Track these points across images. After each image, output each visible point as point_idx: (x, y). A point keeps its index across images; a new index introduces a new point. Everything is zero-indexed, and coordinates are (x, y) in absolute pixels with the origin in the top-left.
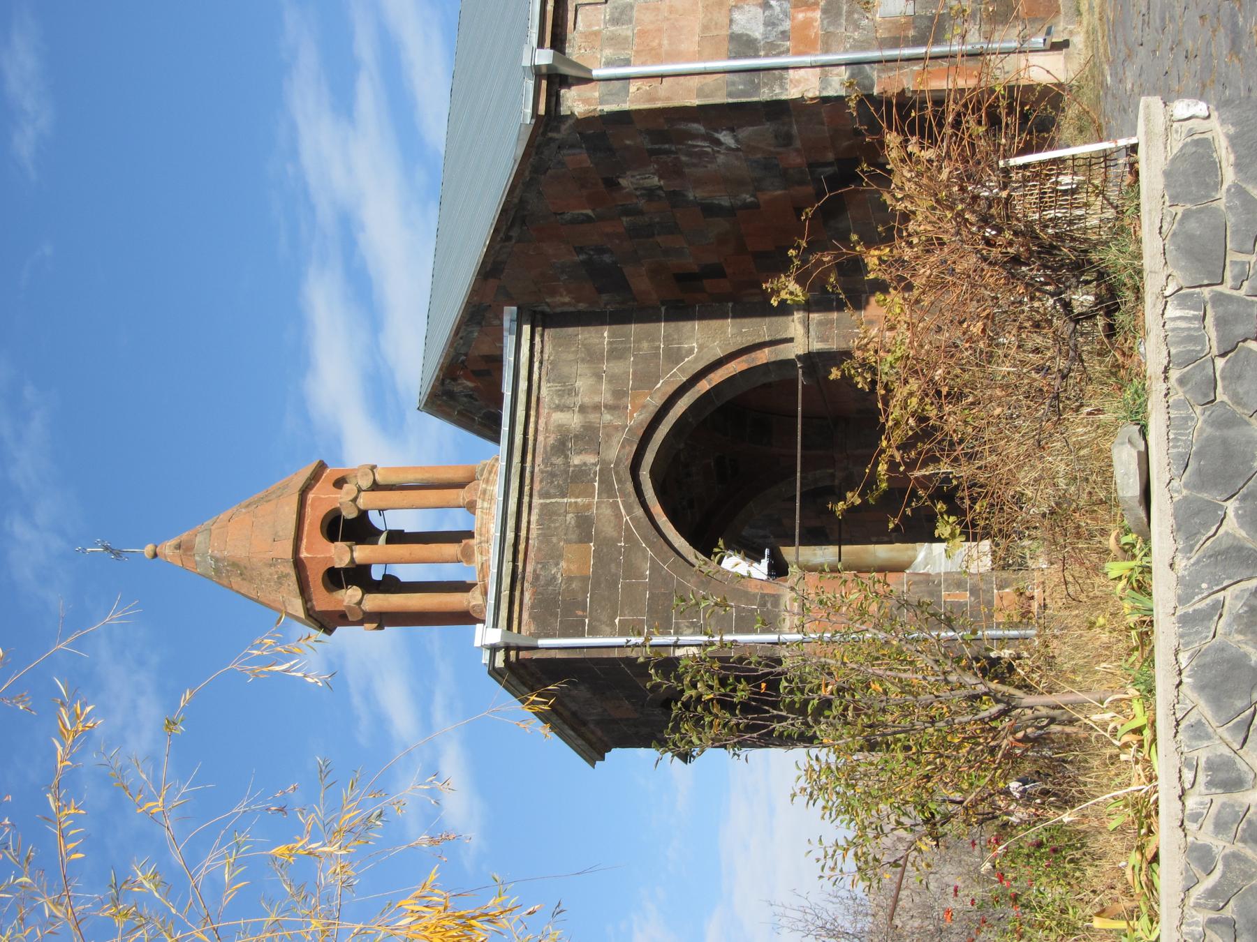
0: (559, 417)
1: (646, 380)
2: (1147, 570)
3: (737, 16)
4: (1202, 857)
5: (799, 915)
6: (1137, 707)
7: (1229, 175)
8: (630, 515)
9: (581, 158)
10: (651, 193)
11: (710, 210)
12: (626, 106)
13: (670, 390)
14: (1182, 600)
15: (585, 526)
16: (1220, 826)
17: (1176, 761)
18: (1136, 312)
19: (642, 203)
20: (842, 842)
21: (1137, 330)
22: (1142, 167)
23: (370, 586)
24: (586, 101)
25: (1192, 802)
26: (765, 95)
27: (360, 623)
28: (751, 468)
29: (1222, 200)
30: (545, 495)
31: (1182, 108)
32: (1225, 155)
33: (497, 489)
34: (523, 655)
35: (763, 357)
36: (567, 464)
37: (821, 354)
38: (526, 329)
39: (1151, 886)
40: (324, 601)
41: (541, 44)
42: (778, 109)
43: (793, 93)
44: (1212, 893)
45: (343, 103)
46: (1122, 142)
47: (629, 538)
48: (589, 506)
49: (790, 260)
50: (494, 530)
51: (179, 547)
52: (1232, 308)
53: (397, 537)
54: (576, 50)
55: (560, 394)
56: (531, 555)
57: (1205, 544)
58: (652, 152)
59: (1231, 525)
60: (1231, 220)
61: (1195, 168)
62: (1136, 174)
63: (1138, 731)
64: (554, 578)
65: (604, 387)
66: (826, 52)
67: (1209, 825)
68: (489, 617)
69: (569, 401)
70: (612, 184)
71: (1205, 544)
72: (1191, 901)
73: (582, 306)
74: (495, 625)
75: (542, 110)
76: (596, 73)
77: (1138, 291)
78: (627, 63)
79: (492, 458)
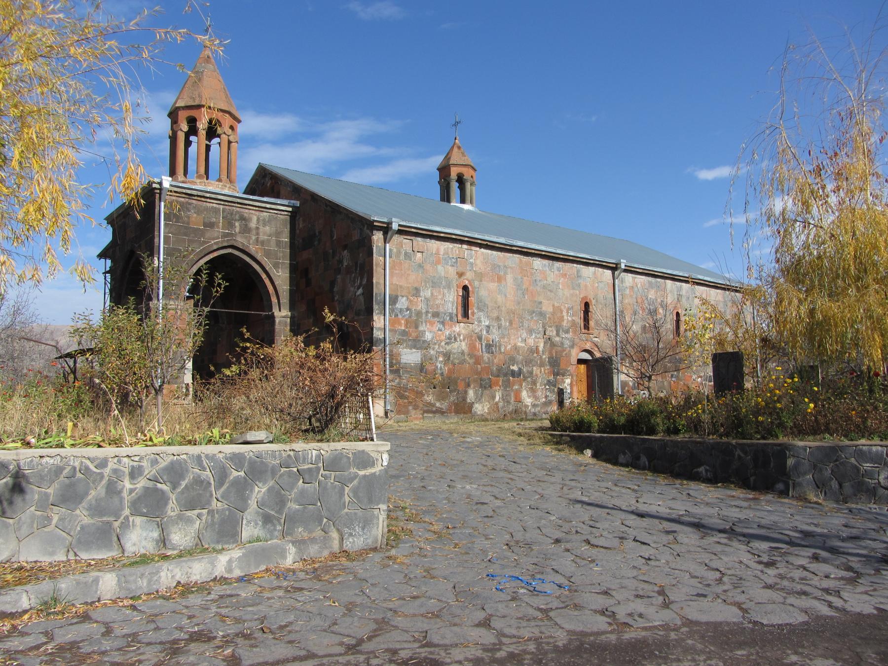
0: (255, 219)
1: (267, 254)
2: (217, 443)
3: (405, 298)
4: (103, 463)
5: (24, 299)
6: (161, 439)
7: (362, 473)
8: (213, 243)
9: (356, 236)
10: (340, 262)
11: (333, 283)
12: (374, 255)
13: (263, 263)
14: (207, 456)
15: (211, 225)
16: (115, 471)
17: (143, 454)
18: (314, 440)
19: (337, 258)
20: (91, 323)
21: (306, 440)
22: (365, 443)
23: (187, 135)
24: (377, 240)
25: (126, 460)
26: (375, 307)
27: (172, 129)
28: (231, 295)
29: (353, 470)
30: (224, 211)
31: (386, 457)
32: (372, 470)
33: (226, 191)
34: (158, 195)
35: (274, 300)
36: (236, 220)
37: (274, 322)
38: (290, 209)
39: (88, 445)
40: (183, 115)
41: (399, 225)
42: (369, 312)
43: (375, 317)
44: (87, 468)
45: (364, 140)
46: (375, 436)
47: (205, 243)
48: (218, 227)
49: (341, 317)
50: (209, 189)
51: (208, 57)
52: (315, 474)
53: (208, 148)
54: (397, 238)
55: (264, 220)
56: (200, 203)
57: (228, 464)
58: (356, 263)
59: (235, 474)
60: (346, 473)
61: (365, 461)
62: (363, 440)
63: (151, 440)
64: (189, 211)
65: (266, 235)
66: (390, 330)
67: (115, 466)
68: (174, 183)
69: (261, 223)
70: (345, 247)
71: (228, 464)
72: (84, 460)
73: (298, 231)
74: (171, 185)
75: (375, 224)
76: (388, 245)
77: (321, 441)
78: (390, 257)
79: (238, 190)
